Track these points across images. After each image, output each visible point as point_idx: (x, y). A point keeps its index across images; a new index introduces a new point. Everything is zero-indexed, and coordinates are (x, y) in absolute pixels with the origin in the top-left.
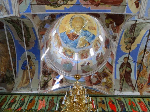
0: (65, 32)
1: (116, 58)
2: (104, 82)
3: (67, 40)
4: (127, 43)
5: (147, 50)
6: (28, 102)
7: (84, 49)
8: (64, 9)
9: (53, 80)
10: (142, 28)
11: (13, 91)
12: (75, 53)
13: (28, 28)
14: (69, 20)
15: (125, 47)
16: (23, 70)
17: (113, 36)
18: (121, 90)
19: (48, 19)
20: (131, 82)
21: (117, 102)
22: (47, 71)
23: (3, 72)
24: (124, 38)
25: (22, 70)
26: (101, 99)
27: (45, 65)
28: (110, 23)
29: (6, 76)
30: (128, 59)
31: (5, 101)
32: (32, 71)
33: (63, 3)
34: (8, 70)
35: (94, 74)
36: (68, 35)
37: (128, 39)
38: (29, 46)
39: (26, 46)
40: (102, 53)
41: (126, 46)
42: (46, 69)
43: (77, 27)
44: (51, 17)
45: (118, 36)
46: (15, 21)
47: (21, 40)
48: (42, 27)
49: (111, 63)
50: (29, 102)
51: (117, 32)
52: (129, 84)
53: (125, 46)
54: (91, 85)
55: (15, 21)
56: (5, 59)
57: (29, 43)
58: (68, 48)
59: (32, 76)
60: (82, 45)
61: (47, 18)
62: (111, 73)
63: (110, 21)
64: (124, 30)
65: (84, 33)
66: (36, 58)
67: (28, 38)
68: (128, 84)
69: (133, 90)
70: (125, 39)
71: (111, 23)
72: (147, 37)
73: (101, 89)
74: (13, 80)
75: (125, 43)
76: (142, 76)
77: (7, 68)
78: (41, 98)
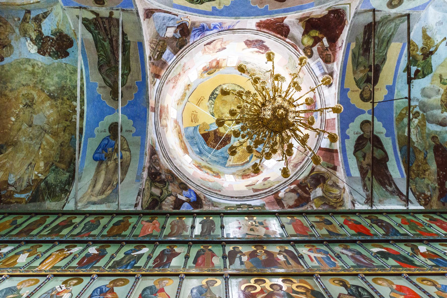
0: (198, 126)
3: (202, 147)
5: (413, 109)
8: (210, 9)
13: (128, 44)
14: (208, 98)
20: (393, 183)
22: (160, 174)
27: (156, 156)
28: (313, 45)
29: (46, 183)
34: (54, 167)
36: (203, 135)
37: (361, 71)
41: (360, 91)
42: (157, 168)
48: (158, 53)
53: (356, 91)
55: (95, 35)
56: (53, 141)
61: (170, 33)
62: (335, 168)
66: (134, 130)
68: (387, 190)
70: (354, 73)
71: (317, 40)
72: (404, 71)
75: (356, 82)
77: (53, 164)
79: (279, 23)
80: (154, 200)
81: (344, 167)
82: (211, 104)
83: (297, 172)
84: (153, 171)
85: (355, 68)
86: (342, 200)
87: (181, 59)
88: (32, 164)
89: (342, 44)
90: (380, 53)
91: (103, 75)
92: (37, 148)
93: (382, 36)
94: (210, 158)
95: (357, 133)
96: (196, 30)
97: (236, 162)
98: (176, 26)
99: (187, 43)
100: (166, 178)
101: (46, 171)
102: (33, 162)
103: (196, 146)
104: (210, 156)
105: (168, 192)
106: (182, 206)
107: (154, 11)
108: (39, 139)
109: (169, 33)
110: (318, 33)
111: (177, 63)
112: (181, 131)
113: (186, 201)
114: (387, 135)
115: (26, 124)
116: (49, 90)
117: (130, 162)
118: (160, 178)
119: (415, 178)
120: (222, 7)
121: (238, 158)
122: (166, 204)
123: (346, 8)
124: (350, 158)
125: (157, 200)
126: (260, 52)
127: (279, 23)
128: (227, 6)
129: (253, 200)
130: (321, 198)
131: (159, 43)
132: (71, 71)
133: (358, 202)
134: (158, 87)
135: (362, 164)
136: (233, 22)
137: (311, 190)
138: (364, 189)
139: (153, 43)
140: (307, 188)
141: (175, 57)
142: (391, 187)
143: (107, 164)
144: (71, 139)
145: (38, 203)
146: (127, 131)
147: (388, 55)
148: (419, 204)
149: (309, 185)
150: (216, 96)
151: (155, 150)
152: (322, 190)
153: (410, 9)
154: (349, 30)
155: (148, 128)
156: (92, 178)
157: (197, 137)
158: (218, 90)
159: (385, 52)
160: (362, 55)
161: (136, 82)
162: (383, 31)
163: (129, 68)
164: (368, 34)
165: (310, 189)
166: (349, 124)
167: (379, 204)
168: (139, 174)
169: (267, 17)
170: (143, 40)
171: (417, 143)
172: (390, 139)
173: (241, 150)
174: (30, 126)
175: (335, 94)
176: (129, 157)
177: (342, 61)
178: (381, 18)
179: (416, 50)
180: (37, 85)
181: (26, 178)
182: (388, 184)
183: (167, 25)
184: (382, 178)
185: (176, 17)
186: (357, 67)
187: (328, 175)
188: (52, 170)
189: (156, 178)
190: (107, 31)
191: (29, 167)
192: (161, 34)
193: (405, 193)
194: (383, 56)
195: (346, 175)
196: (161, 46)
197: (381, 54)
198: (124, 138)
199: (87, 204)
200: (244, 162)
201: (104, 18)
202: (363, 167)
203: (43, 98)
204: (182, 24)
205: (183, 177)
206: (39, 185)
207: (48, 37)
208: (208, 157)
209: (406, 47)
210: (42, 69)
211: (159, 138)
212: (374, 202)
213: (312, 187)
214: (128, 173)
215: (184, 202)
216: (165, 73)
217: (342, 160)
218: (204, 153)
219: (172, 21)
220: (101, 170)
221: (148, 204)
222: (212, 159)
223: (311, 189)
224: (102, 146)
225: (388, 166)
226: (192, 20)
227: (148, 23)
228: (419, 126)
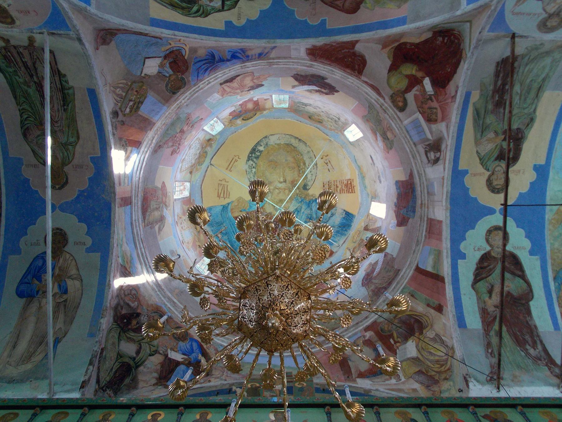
0: (228, 204)
1: (452, 231)
2: (408, 359)
4: (489, 159)
8: (221, 26)
9: (164, 357)
10: (541, 79)
13: (70, 91)
15: (483, 180)
17: (428, 140)
20: (538, 342)
28: (408, 89)
30: (506, 237)
32: (66, 301)
35: (359, 335)
37: (489, 140)
38: (66, 183)
39: (53, 187)
41: (487, 174)
42: (132, 305)
43: (276, 188)
45: (448, 136)
46: (19, 53)
47: (34, 161)
48: (131, 103)
49: (434, 267)
51: (443, 120)
52: (532, 351)
53: (480, 174)
55: (10, 75)
57: (66, 169)
59: (60, 324)
62: (439, 309)
63: (407, 76)
64: (468, 95)
66: (89, 241)
68: (527, 354)
70: (477, 143)
71: (414, 82)
75: (480, 159)
79: (347, 50)
80: (123, 364)
82: (251, 167)
84: (124, 312)
86: (449, 369)
89: (456, 92)
90: (524, 109)
91: (32, 145)
93: (528, 81)
95: (479, 249)
98: (162, 55)
105: (150, 348)
106: (174, 373)
107: (115, 31)
110: (416, 70)
113: (182, 363)
114: (532, 253)
117: (81, 300)
120: (243, 22)
122: (145, 370)
124: (465, 295)
125: (129, 365)
126: (323, 92)
127: (347, 50)
128: (253, 19)
130: (415, 360)
131: (131, 85)
133: (475, 379)
135: (485, 306)
136: (265, 48)
137: (398, 344)
138: (488, 352)
139: (119, 87)
142: (535, 349)
143: (40, 304)
146: (76, 243)
147: (538, 113)
149: (395, 335)
150: (259, 154)
155: (113, 238)
158: (262, 144)
159: (534, 106)
160: (492, 113)
162: (530, 71)
163: (75, 132)
164: (503, 76)
165: (395, 342)
178: (527, 48)
184: (520, 331)
185: (159, 40)
186: (482, 133)
187: (428, 320)
189: (131, 323)
190: (29, 69)
194: (530, 114)
196: (137, 91)
197: (526, 111)
198: (72, 256)
201: (21, 46)
202: (487, 310)
211: (141, 249)
213: (399, 340)
215: (178, 364)
221: (112, 374)
223: (398, 342)
226: (190, 46)
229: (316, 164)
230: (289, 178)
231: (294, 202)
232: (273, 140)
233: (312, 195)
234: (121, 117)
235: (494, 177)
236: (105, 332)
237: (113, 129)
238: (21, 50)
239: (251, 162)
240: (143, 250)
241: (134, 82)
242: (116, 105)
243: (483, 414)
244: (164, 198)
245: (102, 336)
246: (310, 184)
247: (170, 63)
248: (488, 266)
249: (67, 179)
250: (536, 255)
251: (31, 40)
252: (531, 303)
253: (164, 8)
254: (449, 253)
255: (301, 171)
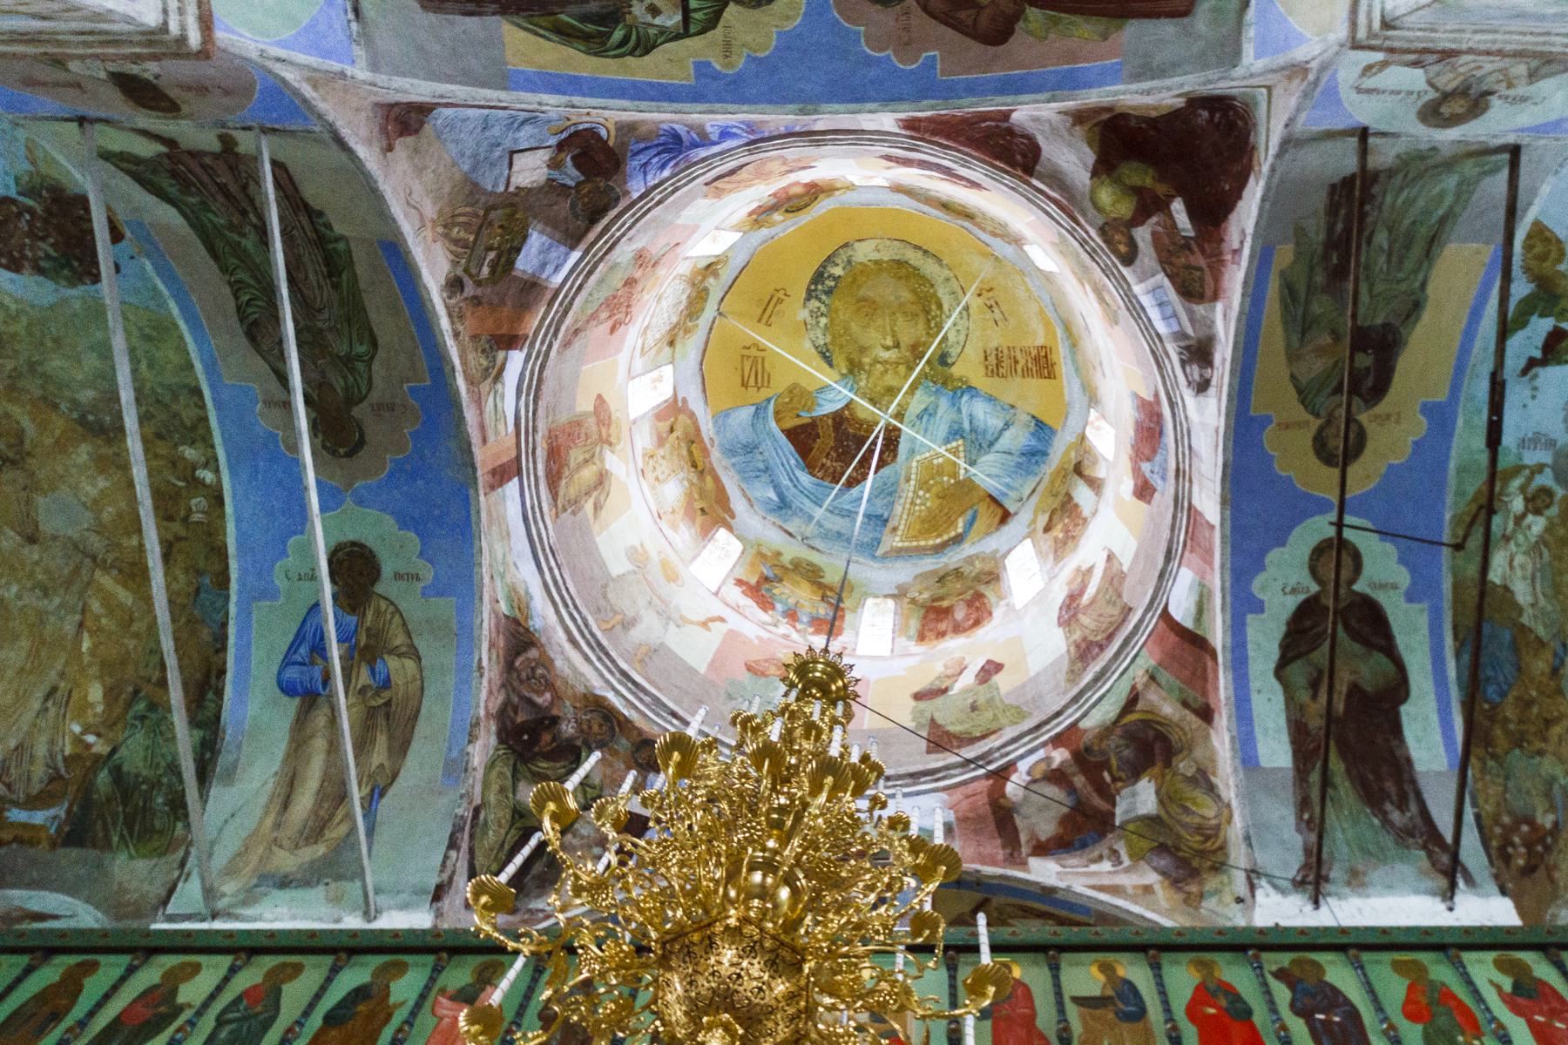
3: (786, 482)
6: (306, 1013)
7: (953, 558)
8: (683, 77)
11: (171, 918)
12: (870, 602)
15: (1305, 438)
16: (297, 701)
18: (1311, 878)
19: (550, 180)
20: (1412, 796)
21: (1282, 994)
22: (555, 721)
23: (86, 731)
24: (1288, 346)
25: (286, 699)
26: (1106, 968)
27: (533, 653)
29: (118, 774)
31: (56, 1017)
32: (388, 704)
33: (678, 17)
35: (1041, 754)
37: (1320, 351)
38: (361, 443)
40: (1110, 558)
41: (1316, 423)
42: (539, 700)
43: (876, 361)
44: (577, 163)
46: (204, 167)
48: (492, 255)
50: (316, 1020)
52: (1396, 816)
53: (1300, 425)
54: (1015, 859)
55: (204, 167)
57: (356, 412)
58: (792, 551)
60: (931, 523)
61: (531, 170)
65: (953, 415)
66: (428, 575)
67: (348, 361)
68: (1386, 822)
69: (1443, 882)
70: (1292, 356)
71: (1148, 205)
73: (1115, 890)
74: (178, 806)
75: (1300, 392)
76: (1518, 741)
77: (136, 692)
78: (459, 975)
81: (1234, 726)
82: (816, 314)
83: (1082, 693)
84: (521, 718)
85: (1295, 338)
87: (606, 253)
88: (59, 693)
89: (1242, 243)
90: (1399, 282)
92: (69, 628)
93: (1407, 222)
94: (819, 524)
95: (1294, 591)
96: (646, 148)
97: (916, 538)
98: (553, 141)
99: (617, 200)
100: (582, 731)
101: (114, 724)
102: (62, 685)
103: (765, 478)
104: (819, 513)
108: (75, 588)
109: (527, 174)
111: (590, 273)
112: (698, 430)
115: (12, 528)
116: (75, 403)
118: (554, 739)
119: (1507, 753)
120: (741, 63)
121: (923, 522)
123: (1254, 97)
129: (918, 793)
130: (1152, 821)
132: (147, 331)
133: (1270, 883)
134: (522, 375)
137: (1119, 784)
139: (459, 224)
140: (1106, 775)
141: (576, 255)
142: (1403, 812)
144: (198, 591)
145: (92, 854)
146: (398, 576)
147: (1430, 289)
148: (1495, 889)
149: (1114, 762)
151: (527, 630)
152: (1157, 793)
153: (1522, 130)
154: (1263, 200)
156: (276, 766)
157: (767, 446)
159: (1421, 277)
161: (412, 390)
162: (1410, 202)
163: (366, 335)
165: (1115, 779)
166: (1263, 552)
167: (1347, 890)
168: (455, 754)
169: (932, 108)
170: (398, 232)
171: (1530, 611)
172: (1422, 611)
173: (934, 490)
174: (32, 540)
175: (1217, 431)
176: (414, 679)
177: (1241, 313)
178: (1398, 156)
179: (1553, 255)
180: (21, 384)
181: (41, 750)
182: (1395, 798)
183: (507, 144)
186: (1303, 332)
188: (135, 718)
191: (49, 704)
192: (491, 181)
193: (1449, 838)
195: (1238, 761)
196: (501, 227)
197: (1403, 287)
198: (392, 603)
199: (256, 886)
200: (946, 537)
202: (1306, 725)
203: (58, 432)
204: (577, 133)
205: (653, 711)
206: (92, 783)
207: (13, 201)
208: (811, 518)
209: (1498, 284)
210: (24, 320)
211: (551, 569)
212: (1327, 880)
213: (1123, 775)
214: (415, 746)
216: (544, 319)
217: (1227, 698)
218: (796, 503)
219: (528, 130)
220: (312, 736)
222: (828, 525)
223: (1120, 779)
224: (309, 636)
225: (1405, 720)
227: (416, 151)
228: (1546, 544)
229: (967, 308)
230: (906, 339)
231: (918, 393)
232: (864, 253)
233: (960, 379)
234: (470, 290)
235: (1331, 431)
236: (480, 774)
237: (452, 323)
238: (207, 160)
239: (814, 304)
240: (556, 572)
241: (494, 207)
242: (455, 264)
243: (1274, 968)
244: (604, 431)
245: (475, 784)
246: (954, 352)
247: (573, 158)
248: (1313, 627)
249: (362, 435)
250: (1420, 601)
251: (228, 142)
252: (1405, 709)
253: (541, 40)
254: (1228, 599)
255: (932, 325)
